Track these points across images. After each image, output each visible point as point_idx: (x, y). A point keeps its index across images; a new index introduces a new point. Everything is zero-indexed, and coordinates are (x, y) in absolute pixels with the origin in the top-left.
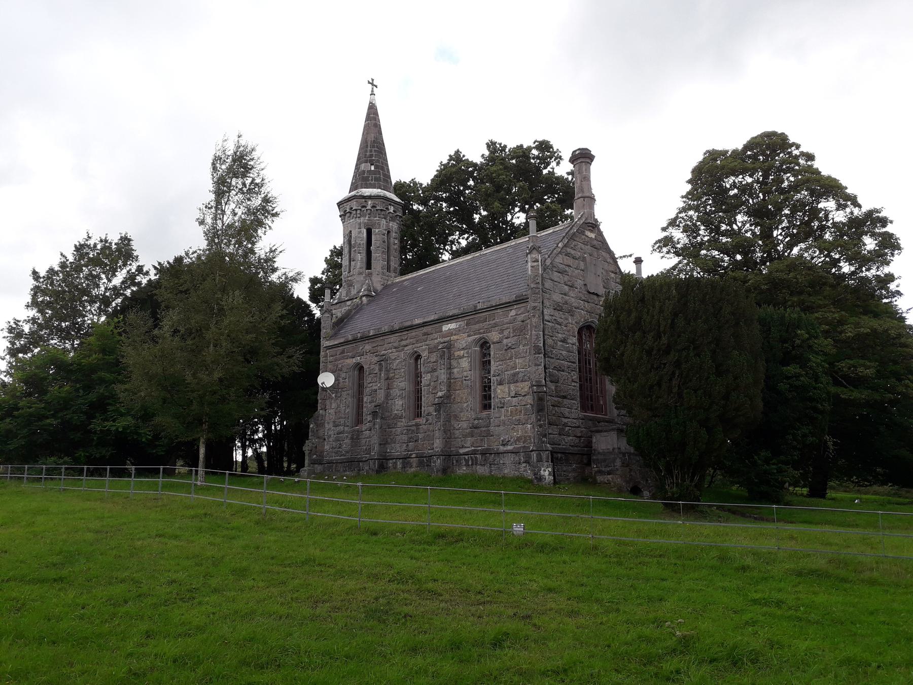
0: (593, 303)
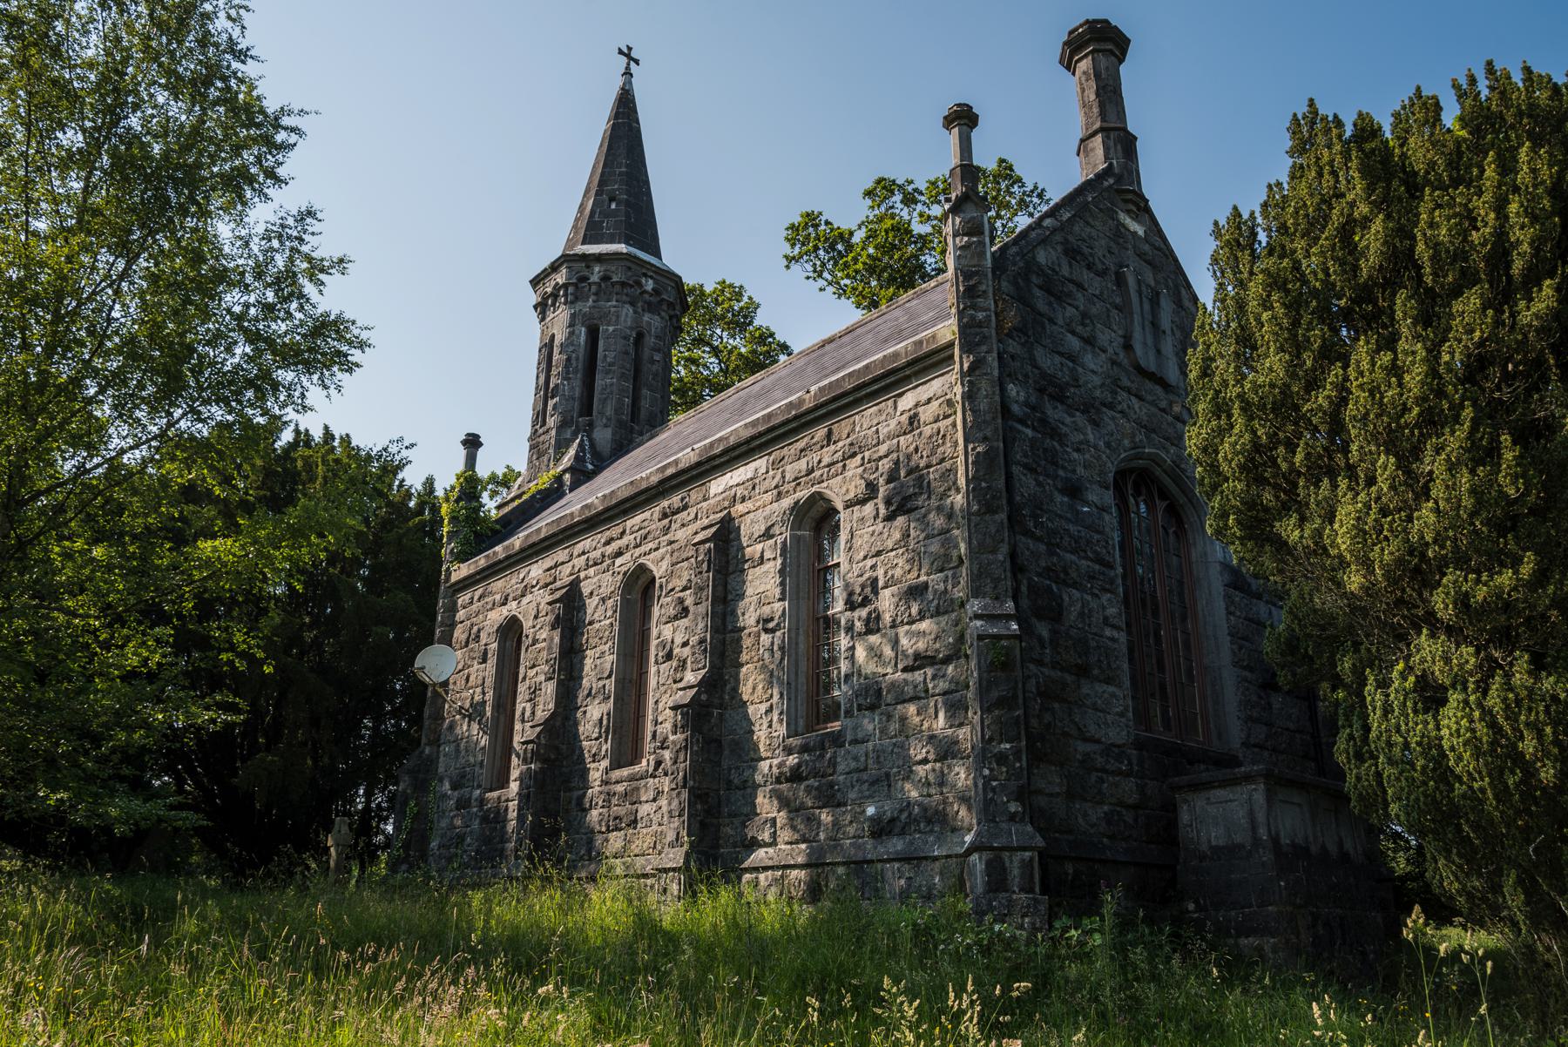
0: (1153, 403)
